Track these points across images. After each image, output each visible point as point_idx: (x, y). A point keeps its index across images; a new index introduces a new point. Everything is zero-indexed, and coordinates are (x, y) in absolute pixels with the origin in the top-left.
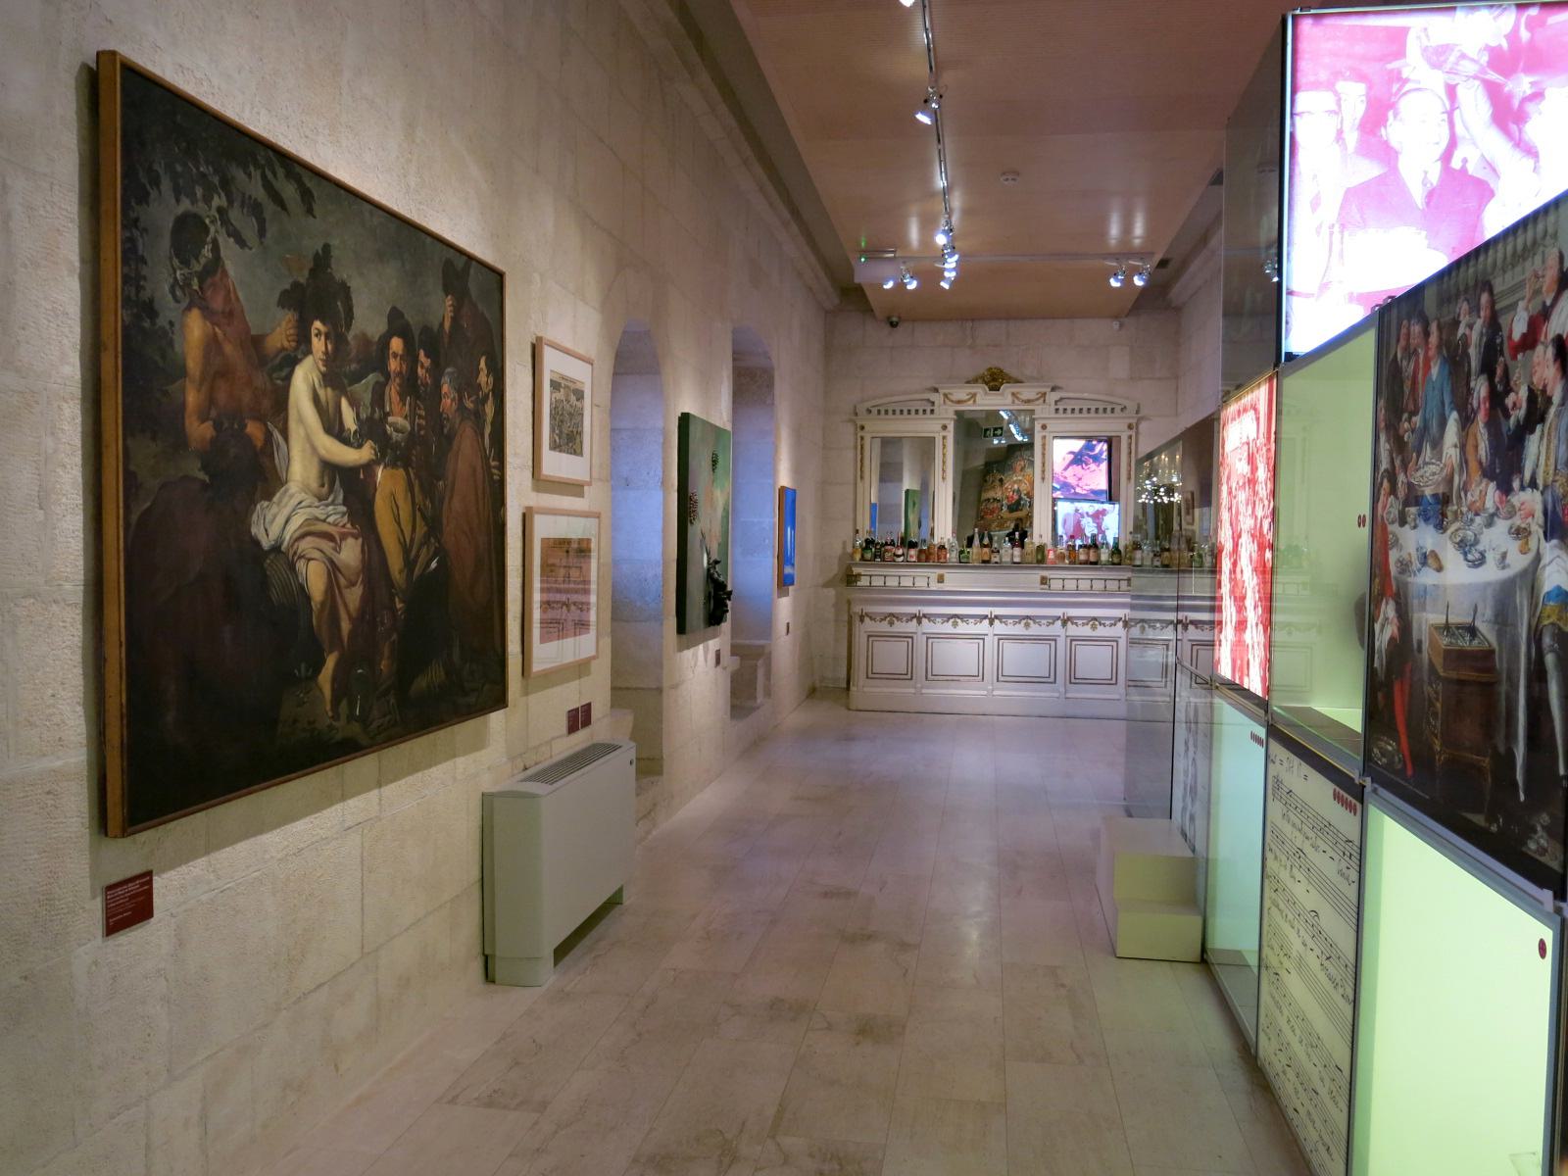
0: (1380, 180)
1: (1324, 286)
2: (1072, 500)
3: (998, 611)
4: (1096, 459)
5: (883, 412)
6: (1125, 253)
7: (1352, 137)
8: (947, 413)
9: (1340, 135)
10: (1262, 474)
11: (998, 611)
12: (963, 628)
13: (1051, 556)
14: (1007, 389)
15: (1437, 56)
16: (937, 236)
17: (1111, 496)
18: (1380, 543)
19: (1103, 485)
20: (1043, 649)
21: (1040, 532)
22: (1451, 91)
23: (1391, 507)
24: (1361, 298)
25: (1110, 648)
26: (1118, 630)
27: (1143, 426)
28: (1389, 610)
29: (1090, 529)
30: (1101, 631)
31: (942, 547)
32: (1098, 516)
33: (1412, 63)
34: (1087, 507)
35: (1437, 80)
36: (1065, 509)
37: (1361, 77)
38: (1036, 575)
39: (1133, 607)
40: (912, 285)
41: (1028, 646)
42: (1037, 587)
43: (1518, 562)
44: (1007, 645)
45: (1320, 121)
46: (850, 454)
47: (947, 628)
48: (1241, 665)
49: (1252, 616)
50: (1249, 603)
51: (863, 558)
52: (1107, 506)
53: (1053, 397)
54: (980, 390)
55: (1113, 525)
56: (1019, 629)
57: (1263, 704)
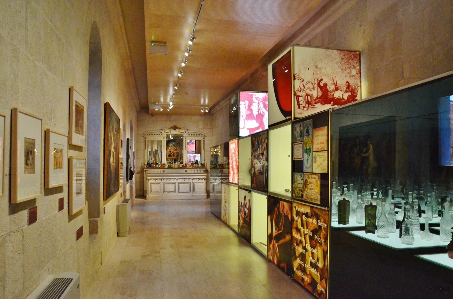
1: (244, 127)
4: (192, 143)
6: (204, 106)
7: (247, 108)
8: (164, 135)
9: (245, 108)
10: (237, 152)
12: (171, 181)
13: (188, 166)
14: (177, 130)
15: (257, 98)
16: (168, 99)
18: (252, 162)
19: (194, 150)
20: (188, 185)
21: (185, 161)
22: (259, 103)
23: (253, 157)
28: (253, 169)
30: (200, 181)
31: (164, 164)
33: (254, 99)
34: (191, 155)
35: (257, 101)
36: (188, 155)
37: (247, 100)
40: (162, 110)
41: (185, 185)
43: (264, 163)
44: (181, 185)
45: (243, 106)
46: (143, 144)
47: (168, 181)
48: (234, 179)
49: (235, 172)
50: (235, 170)
51: (147, 167)
52: (196, 155)
53: (187, 132)
54: (172, 130)
56: (183, 181)
57: (238, 184)
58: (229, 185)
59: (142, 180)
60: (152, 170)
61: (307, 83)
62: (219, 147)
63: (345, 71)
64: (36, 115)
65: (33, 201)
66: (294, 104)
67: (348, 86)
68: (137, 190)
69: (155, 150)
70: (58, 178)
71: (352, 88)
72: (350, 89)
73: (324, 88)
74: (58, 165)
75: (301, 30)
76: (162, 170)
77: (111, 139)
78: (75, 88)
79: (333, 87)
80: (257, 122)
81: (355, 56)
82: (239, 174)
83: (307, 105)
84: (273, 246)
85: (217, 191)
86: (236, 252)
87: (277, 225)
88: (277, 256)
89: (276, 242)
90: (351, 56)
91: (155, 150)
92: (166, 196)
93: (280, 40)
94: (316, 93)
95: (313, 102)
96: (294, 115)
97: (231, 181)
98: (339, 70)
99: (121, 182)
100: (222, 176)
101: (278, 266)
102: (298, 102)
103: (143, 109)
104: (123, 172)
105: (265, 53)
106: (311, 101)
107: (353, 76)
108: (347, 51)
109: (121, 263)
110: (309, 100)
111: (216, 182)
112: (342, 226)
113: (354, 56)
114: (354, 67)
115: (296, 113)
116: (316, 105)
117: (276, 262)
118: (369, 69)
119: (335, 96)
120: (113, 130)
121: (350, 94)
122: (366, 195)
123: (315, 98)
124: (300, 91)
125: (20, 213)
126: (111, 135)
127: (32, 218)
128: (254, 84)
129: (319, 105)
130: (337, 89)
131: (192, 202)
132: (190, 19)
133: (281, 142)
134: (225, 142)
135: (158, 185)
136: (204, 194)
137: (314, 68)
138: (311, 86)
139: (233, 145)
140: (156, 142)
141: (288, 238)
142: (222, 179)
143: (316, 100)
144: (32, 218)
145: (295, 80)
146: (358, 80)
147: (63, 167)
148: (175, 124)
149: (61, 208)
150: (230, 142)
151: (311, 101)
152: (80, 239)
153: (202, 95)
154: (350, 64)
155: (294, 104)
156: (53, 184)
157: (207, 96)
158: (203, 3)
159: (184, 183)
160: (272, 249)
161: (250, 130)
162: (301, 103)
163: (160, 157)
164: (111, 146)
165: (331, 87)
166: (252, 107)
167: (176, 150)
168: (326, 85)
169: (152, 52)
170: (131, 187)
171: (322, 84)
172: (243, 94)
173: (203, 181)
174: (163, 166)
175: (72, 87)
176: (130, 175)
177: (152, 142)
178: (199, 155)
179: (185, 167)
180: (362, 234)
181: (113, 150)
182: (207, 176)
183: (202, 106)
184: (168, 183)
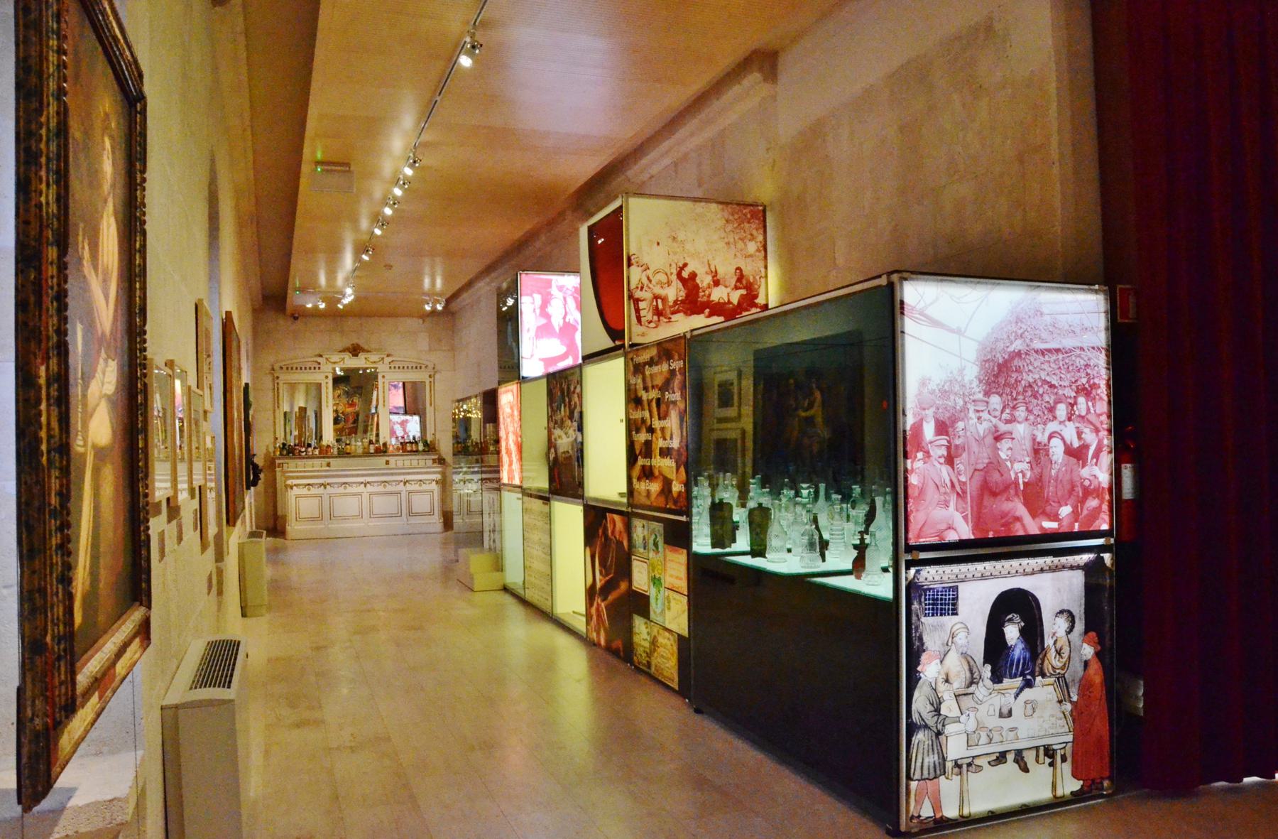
5: (289, 369)
6: (432, 293)
7: (538, 311)
10: (516, 413)
12: (350, 490)
14: (362, 356)
15: (561, 288)
16: (338, 278)
19: (401, 404)
20: (394, 499)
23: (552, 424)
27: (437, 376)
30: (424, 487)
31: (328, 446)
32: (403, 424)
33: (554, 291)
34: (395, 418)
37: (539, 293)
38: (384, 459)
44: (375, 498)
46: (271, 394)
47: (341, 490)
48: (511, 478)
52: (408, 417)
53: (388, 360)
54: (347, 356)
56: (381, 489)
58: (499, 490)
59: (271, 490)
60: (300, 462)
61: (656, 272)
62: (474, 400)
66: (629, 316)
69: (300, 408)
71: (748, 281)
73: (689, 283)
80: (563, 343)
81: (754, 215)
82: (520, 465)
83: (656, 318)
84: (598, 610)
85: (469, 512)
86: (520, 632)
87: (603, 564)
88: (605, 630)
91: (300, 408)
92: (336, 527)
94: (674, 292)
97: (505, 480)
98: (721, 245)
100: (482, 472)
101: (608, 649)
102: (638, 311)
105: (572, 190)
107: (751, 256)
109: (269, 660)
110: (660, 306)
111: (468, 486)
112: (718, 550)
113: (750, 213)
114: (753, 238)
116: (674, 317)
117: (603, 642)
119: (713, 298)
121: (743, 292)
129: (679, 317)
130: (717, 283)
131: (410, 538)
133: (605, 392)
134: (489, 387)
135: (316, 501)
136: (436, 522)
138: (663, 278)
139: (507, 398)
140: (302, 388)
141: (623, 586)
146: (761, 264)
148: (355, 341)
150: (502, 390)
153: (427, 270)
155: (629, 316)
157: (439, 271)
158: (438, 98)
159: (386, 493)
160: (595, 617)
161: (548, 362)
162: (642, 313)
163: (312, 425)
165: (704, 280)
167: (352, 405)
168: (693, 276)
171: (685, 274)
172: (528, 280)
173: (434, 486)
177: (293, 387)
178: (416, 418)
179: (382, 451)
180: (747, 560)
182: (443, 474)
183: (424, 294)
184: (346, 495)
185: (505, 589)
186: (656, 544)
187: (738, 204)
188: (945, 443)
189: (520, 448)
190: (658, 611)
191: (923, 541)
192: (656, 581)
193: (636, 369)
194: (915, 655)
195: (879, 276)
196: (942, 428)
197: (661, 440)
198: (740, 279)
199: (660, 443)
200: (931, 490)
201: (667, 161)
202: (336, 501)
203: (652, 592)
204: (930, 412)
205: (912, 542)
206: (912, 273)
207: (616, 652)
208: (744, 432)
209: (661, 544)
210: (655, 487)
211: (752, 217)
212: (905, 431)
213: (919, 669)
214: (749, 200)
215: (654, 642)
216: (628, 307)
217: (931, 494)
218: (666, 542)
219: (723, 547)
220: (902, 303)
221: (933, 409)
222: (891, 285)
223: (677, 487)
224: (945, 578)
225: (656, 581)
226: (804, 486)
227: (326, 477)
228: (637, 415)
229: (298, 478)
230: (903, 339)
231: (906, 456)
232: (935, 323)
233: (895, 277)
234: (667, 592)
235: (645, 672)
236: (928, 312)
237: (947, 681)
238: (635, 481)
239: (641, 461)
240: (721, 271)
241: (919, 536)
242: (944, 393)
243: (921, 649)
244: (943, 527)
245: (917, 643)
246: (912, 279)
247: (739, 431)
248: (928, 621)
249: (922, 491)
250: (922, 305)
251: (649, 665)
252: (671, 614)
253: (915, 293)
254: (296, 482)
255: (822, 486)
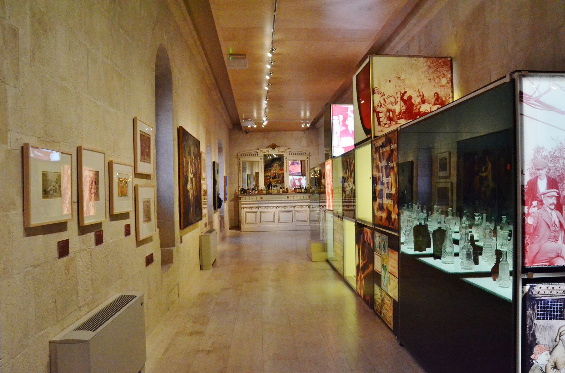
0: (345, 130)
2: (292, 175)
3: (278, 205)
4: (297, 163)
5: (245, 155)
6: (305, 119)
7: (341, 123)
8: (261, 155)
11: (278, 205)
12: (269, 210)
14: (276, 149)
16: (261, 114)
17: (303, 174)
19: (300, 171)
20: (289, 213)
24: (345, 148)
25: (304, 219)
26: (307, 208)
29: (298, 183)
30: (303, 209)
31: (262, 190)
32: (299, 180)
34: (296, 177)
36: (291, 178)
37: (341, 114)
39: (310, 202)
40: (255, 126)
41: (285, 213)
42: (286, 199)
44: (280, 213)
47: (266, 210)
48: (329, 206)
52: (302, 177)
54: (270, 149)
55: (304, 182)
56: (283, 209)
60: (247, 197)
63: (433, 81)
64: (100, 149)
65: (99, 225)
66: (374, 121)
67: (437, 97)
68: (231, 220)
70: (122, 205)
71: (442, 100)
72: (440, 101)
73: (408, 102)
74: (123, 193)
75: (396, 32)
76: (259, 197)
77: (187, 164)
78: (138, 118)
79: (419, 100)
81: (445, 63)
83: (389, 122)
87: (362, 255)
89: (363, 273)
90: (440, 63)
92: (263, 226)
93: (371, 46)
94: (399, 108)
95: (396, 118)
96: (374, 133)
98: (426, 80)
99: (205, 211)
100: (320, 202)
101: (364, 299)
102: (378, 118)
103: (235, 127)
104: (208, 201)
106: (393, 117)
108: (436, 58)
110: (391, 115)
114: (445, 76)
115: (376, 131)
118: (461, 76)
119: (421, 110)
120: (190, 154)
122: (449, 219)
123: (397, 114)
124: (381, 106)
125: (88, 235)
126: (187, 161)
127: (99, 240)
128: (341, 97)
130: (423, 102)
131: (296, 232)
132: (268, 29)
135: (254, 215)
137: (397, 79)
138: (393, 100)
139: (328, 167)
142: (320, 206)
143: (399, 115)
144: (99, 240)
145: (375, 95)
146: (450, 91)
147: (128, 194)
148: (274, 143)
149: (128, 233)
150: (326, 163)
151: (393, 117)
152: (150, 265)
153: (302, 108)
154: (440, 73)
155: (374, 121)
156: (116, 211)
157: (308, 108)
158: (275, 14)
159: (285, 211)
162: (381, 119)
164: (187, 171)
165: (416, 100)
166: (347, 123)
168: (410, 98)
169: (231, 65)
170: (222, 218)
171: (405, 97)
172: (336, 108)
174: (260, 193)
175: (136, 118)
176: (217, 203)
179: (286, 192)
180: (430, 261)
181: (190, 176)
183: (302, 120)
185: (327, 261)
186: (384, 247)
187: (436, 58)
188: (555, 194)
189: (332, 191)
190: (385, 284)
191: (536, 265)
192: (384, 267)
193: (375, 150)
194: (530, 345)
195: (505, 77)
196: (552, 184)
197: (387, 189)
198: (437, 99)
199: (386, 191)
200: (543, 228)
201: (404, 42)
202: (263, 214)
203: (383, 273)
204: (543, 172)
205: (528, 266)
206: (530, 71)
207: (368, 303)
208: (452, 184)
209: (386, 247)
210: (384, 215)
211: (444, 63)
212: (523, 186)
213: (532, 357)
214: (443, 55)
215: (383, 300)
216: (373, 116)
217: (544, 231)
218: (389, 247)
219: (421, 251)
220: (521, 93)
221: (546, 170)
222: (513, 81)
223: (394, 216)
224: (554, 292)
225: (384, 267)
226: (476, 214)
227: (258, 204)
228: (376, 174)
229: (246, 204)
230: (522, 120)
231: (524, 204)
232: (548, 107)
233: (516, 75)
234: (389, 275)
235: (378, 314)
236: (541, 99)
237: (555, 367)
238: (376, 211)
239: (379, 200)
240: (426, 95)
241: (533, 262)
242: (555, 158)
243: (534, 342)
244: (553, 255)
245: (531, 339)
246: (530, 76)
247: (450, 184)
248: (540, 323)
249: (536, 229)
250: (537, 94)
251: (381, 313)
252: (390, 288)
253: (530, 86)
254: (245, 206)
255: (485, 216)
